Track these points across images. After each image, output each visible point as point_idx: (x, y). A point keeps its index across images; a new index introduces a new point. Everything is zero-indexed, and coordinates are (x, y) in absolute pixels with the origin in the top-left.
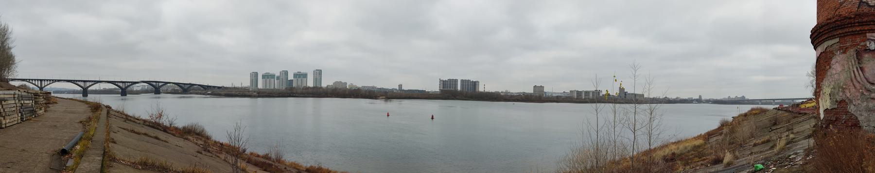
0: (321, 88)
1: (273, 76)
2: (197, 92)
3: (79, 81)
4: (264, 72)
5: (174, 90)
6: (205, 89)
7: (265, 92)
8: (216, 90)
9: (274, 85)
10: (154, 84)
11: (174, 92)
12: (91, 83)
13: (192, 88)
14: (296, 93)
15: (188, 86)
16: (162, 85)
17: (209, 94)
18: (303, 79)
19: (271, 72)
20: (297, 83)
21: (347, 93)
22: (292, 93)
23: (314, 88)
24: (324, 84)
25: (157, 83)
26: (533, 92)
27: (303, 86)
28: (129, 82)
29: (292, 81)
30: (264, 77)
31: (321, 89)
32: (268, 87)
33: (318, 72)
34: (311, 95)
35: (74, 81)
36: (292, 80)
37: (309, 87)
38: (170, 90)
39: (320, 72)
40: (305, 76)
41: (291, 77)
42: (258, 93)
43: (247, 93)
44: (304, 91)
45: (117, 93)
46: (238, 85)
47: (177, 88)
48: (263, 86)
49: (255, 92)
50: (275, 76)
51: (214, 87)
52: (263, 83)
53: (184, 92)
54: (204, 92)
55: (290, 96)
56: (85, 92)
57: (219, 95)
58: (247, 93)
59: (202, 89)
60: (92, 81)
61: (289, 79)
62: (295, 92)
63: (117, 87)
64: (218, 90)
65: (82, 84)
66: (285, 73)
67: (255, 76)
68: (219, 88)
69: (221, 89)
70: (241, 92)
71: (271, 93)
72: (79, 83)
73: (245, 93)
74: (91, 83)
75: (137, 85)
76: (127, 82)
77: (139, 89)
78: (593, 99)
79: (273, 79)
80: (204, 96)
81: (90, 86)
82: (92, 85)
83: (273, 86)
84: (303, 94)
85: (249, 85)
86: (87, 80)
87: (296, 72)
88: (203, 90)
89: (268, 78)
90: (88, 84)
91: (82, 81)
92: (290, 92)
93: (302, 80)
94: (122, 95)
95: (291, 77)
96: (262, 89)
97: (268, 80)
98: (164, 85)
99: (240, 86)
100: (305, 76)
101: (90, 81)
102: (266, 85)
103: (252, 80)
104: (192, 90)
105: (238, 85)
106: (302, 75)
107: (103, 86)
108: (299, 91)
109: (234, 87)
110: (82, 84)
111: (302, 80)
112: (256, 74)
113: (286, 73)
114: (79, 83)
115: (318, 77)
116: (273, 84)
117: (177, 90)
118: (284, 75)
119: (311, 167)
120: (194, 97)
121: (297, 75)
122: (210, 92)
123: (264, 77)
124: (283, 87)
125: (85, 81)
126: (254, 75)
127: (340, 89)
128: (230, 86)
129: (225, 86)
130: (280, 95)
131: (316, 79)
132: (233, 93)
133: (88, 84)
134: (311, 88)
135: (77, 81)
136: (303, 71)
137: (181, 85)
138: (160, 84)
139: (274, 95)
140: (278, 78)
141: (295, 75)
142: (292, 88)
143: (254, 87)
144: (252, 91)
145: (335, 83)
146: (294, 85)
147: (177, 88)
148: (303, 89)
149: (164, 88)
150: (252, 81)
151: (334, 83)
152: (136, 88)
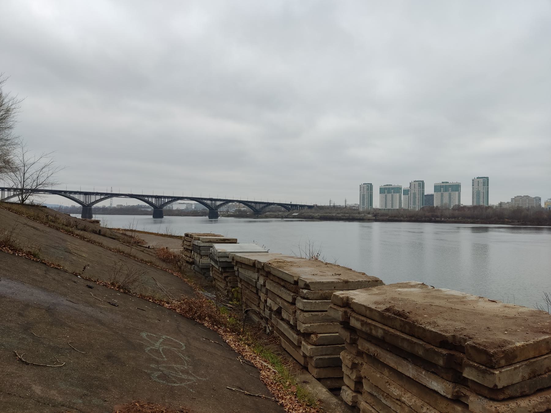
0: (491, 207)
1: (398, 190)
2: (276, 214)
3: (75, 193)
4: (383, 184)
5: (239, 211)
6: (289, 210)
8: (306, 212)
10: (209, 202)
11: (239, 215)
12: (98, 197)
13: (267, 209)
14: (442, 216)
15: (261, 205)
16: (221, 205)
17: (294, 217)
18: (453, 193)
22: (433, 216)
24: (494, 201)
27: (452, 206)
29: (432, 196)
30: (382, 190)
31: (489, 210)
32: (389, 207)
33: (481, 180)
34: (469, 220)
37: (465, 207)
38: (232, 211)
39: (486, 181)
40: (457, 188)
41: (429, 190)
42: (375, 215)
43: (357, 215)
44: (457, 213)
45: (146, 213)
46: (339, 202)
47: (244, 208)
48: (81, 214)
49: (369, 213)
50: (401, 189)
51: (302, 206)
52: (381, 201)
53: (255, 214)
54: (286, 214)
55: (430, 221)
56: (87, 210)
57: (311, 218)
59: (283, 209)
60: (102, 194)
61: (425, 194)
63: (147, 205)
64: (309, 210)
65: (81, 198)
66: (419, 185)
67: (368, 189)
68: (310, 207)
69: (313, 210)
70: (345, 213)
71: (395, 217)
72: (76, 196)
74: (98, 197)
75: (180, 201)
76: (165, 197)
77: (183, 207)
78: (91, 195)
79: (398, 195)
81: (97, 201)
82: (101, 200)
83: (390, 205)
84: (455, 218)
86: (182, 196)
87: (439, 181)
88: (284, 212)
89: (389, 192)
90: (93, 198)
91: (80, 193)
92: (430, 214)
95: (429, 190)
97: (389, 196)
98: (224, 204)
99: (342, 204)
100: (457, 188)
101: (97, 194)
102: (478, 199)
103: (364, 195)
104: (269, 211)
106: (450, 186)
107: (116, 202)
109: (334, 206)
110: (81, 198)
112: (370, 187)
113: (421, 184)
114: (76, 196)
116: (398, 202)
117: (244, 211)
120: (272, 221)
121: (441, 187)
123: (382, 190)
124: (417, 207)
125: (86, 194)
127: (528, 209)
129: (319, 204)
130: (413, 219)
131: (478, 193)
132: (334, 215)
133: (93, 198)
134: (469, 208)
135: (71, 192)
136: (452, 180)
137: (249, 204)
138: (218, 203)
139: (402, 219)
140: (406, 192)
141: (437, 188)
142: (433, 209)
143: (366, 206)
144: (363, 212)
145: (515, 199)
147: (244, 208)
148: (454, 209)
149: (223, 209)
150: (362, 197)
152: (176, 206)
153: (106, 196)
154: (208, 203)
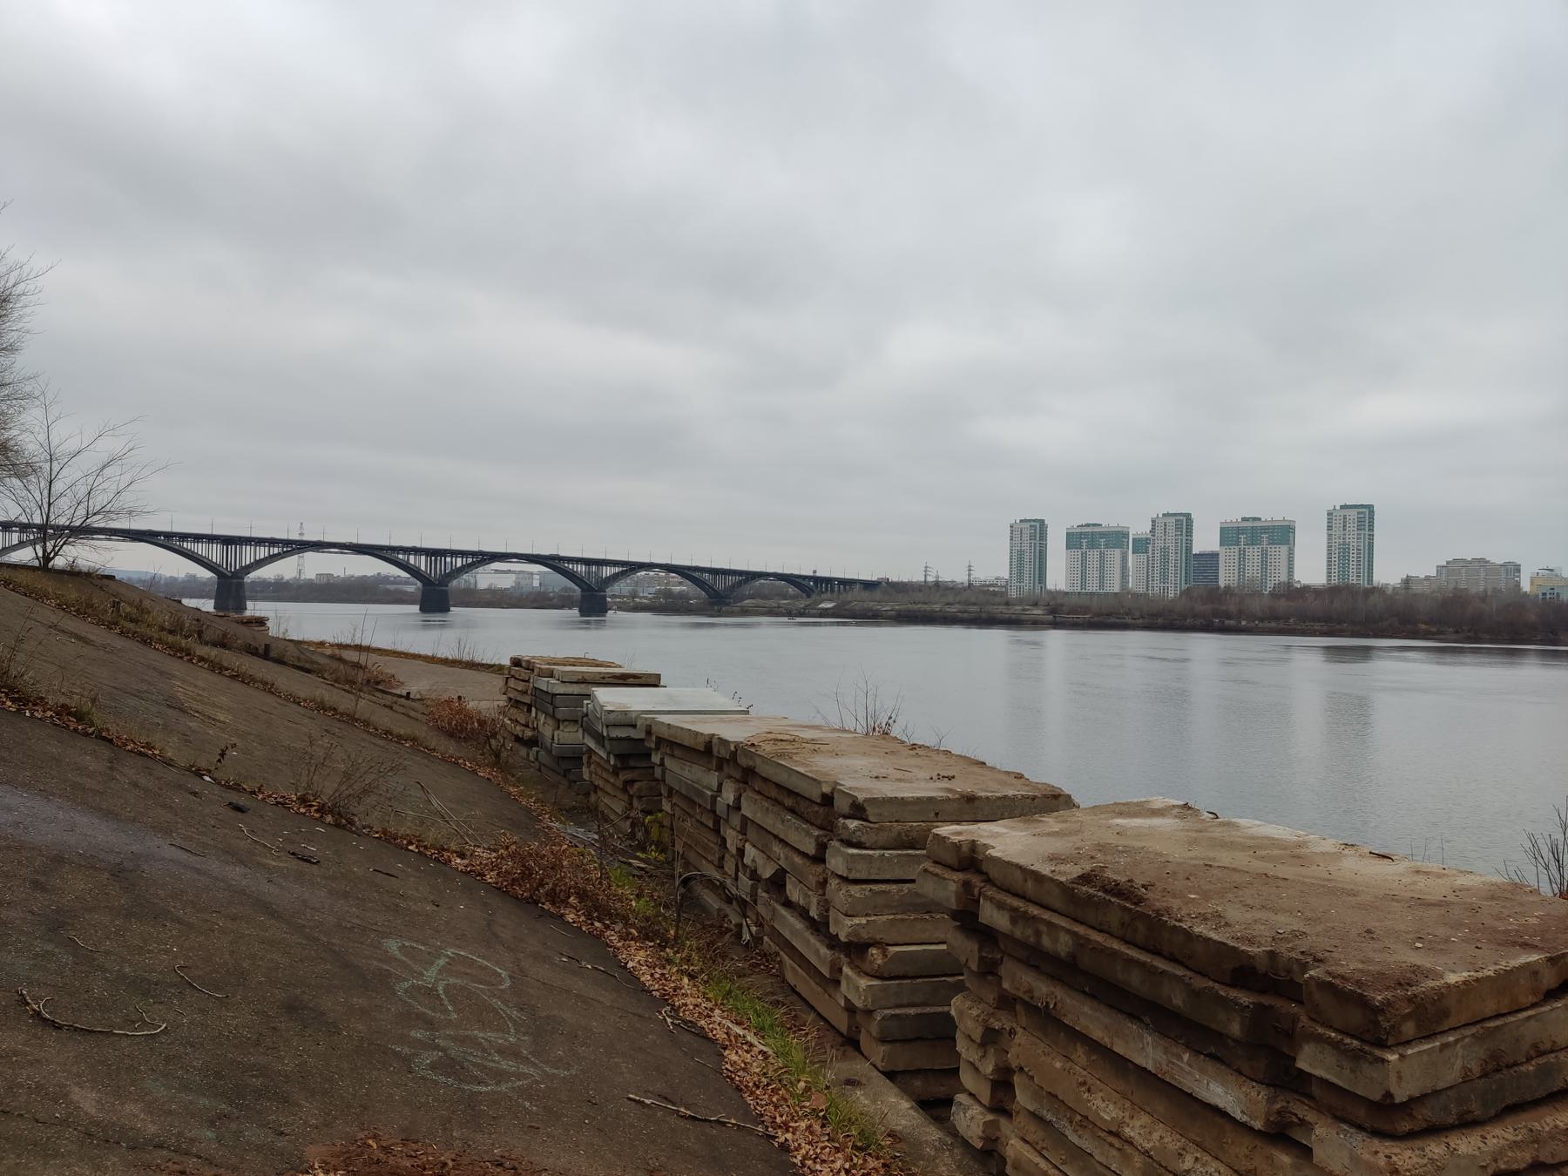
0: (1380, 591)
1: (1117, 538)
2: (772, 603)
3: (198, 538)
4: (1075, 521)
5: (668, 594)
6: (808, 592)
7: (1086, 610)
8: (857, 599)
9: (1124, 576)
10: (581, 569)
11: (668, 605)
12: (263, 552)
13: (747, 589)
14: (1241, 614)
17: (824, 613)
18: (1272, 549)
19: (1109, 519)
20: (1241, 570)
21: (1532, 618)
22: (1215, 614)
23: (1332, 591)
24: (1388, 571)
25: (594, 568)
26: (213, 601)
28: (463, 554)
30: (1074, 540)
32: (1093, 587)
33: (1353, 514)
34: (1317, 626)
35: (169, 535)
36: (1215, 556)
37: (1306, 589)
38: (647, 593)
39: (1365, 516)
40: (1283, 534)
43: (1002, 609)
45: (399, 598)
47: (680, 586)
49: (1036, 604)
50: (1126, 535)
52: (1070, 570)
53: (712, 604)
54: (801, 604)
55: (1208, 628)
56: (231, 587)
57: (870, 617)
58: (1000, 611)
59: (792, 590)
60: (273, 542)
62: (1232, 608)
64: (866, 595)
65: (215, 553)
67: (1033, 537)
68: (869, 585)
69: (878, 594)
72: (200, 549)
73: (990, 608)
74: (263, 552)
77: (506, 582)
79: (1117, 552)
80: (785, 619)
81: (259, 564)
82: (272, 558)
84: (1277, 618)
85: (1007, 576)
87: (1234, 516)
88: (795, 597)
90: (248, 555)
91: (211, 539)
92: (1208, 607)
93: (1264, 554)
94: (583, 613)
95: (1205, 540)
96: (1067, 593)
97: (1094, 555)
100: (1283, 534)
101: (260, 542)
103: (1021, 553)
105: (954, 574)
106: (1265, 529)
107: (313, 566)
108: (1255, 606)
109: (937, 584)
110: (215, 553)
111: (1264, 554)
112: (1038, 530)
113: (1184, 524)
114: (200, 549)
115: (1353, 542)
117: (682, 596)
118: (1171, 530)
119: (1295, 853)
120: (759, 624)
121: (1240, 531)
122: (829, 605)
123: (1074, 540)
124: (1171, 588)
125: (227, 541)
126: (1026, 534)
127: (1484, 598)
128: (918, 577)
130: (1160, 621)
131: (1344, 551)
132: (937, 607)
133: (248, 555)
134: (1317, 592)
135: (184, 537)
136: (1270, 513)
137: (697, 574)
138: (607, 571)
140: (1141, 545)
141: (1229, 535)
142: (1216, 595)
143: (1027, 585)
144: (1020, 601)
145: (1449, 568)
146: (1226, 577)
147: (680, 586)
148: (1274, 595)
149: (622, 587)
150: (1017, 559)
151: (1440, 568)
152: (485, 578)
153: (285, 549)
154: (577, 572)
